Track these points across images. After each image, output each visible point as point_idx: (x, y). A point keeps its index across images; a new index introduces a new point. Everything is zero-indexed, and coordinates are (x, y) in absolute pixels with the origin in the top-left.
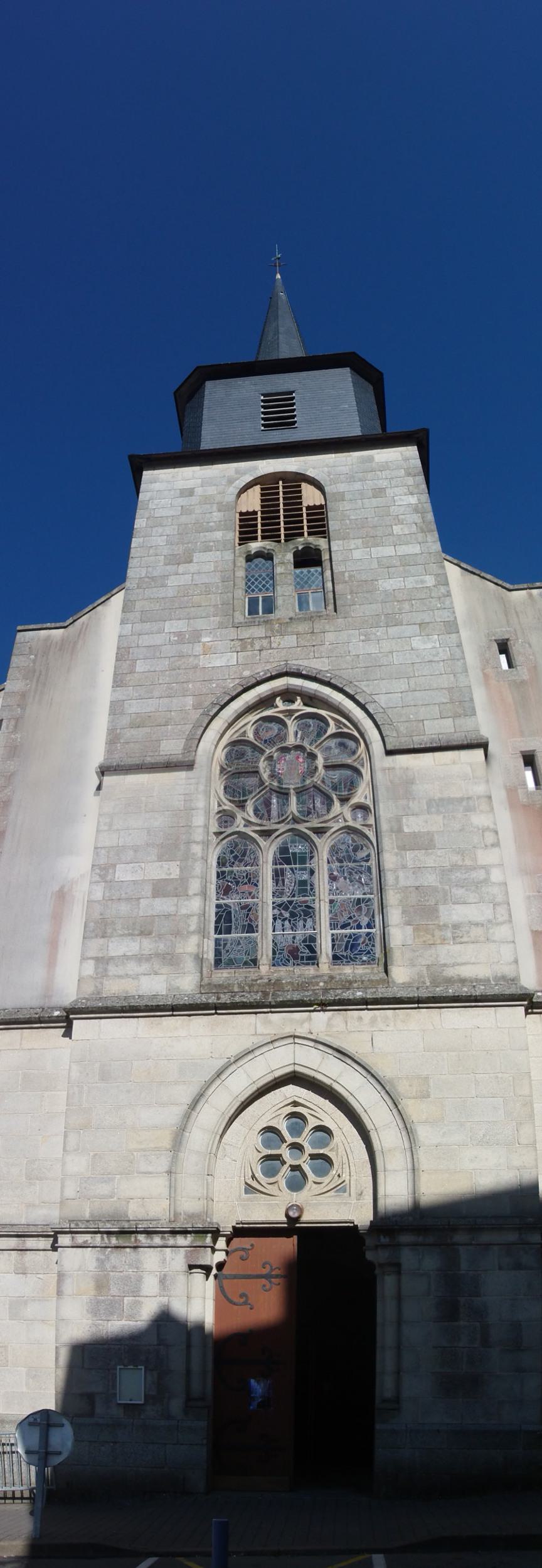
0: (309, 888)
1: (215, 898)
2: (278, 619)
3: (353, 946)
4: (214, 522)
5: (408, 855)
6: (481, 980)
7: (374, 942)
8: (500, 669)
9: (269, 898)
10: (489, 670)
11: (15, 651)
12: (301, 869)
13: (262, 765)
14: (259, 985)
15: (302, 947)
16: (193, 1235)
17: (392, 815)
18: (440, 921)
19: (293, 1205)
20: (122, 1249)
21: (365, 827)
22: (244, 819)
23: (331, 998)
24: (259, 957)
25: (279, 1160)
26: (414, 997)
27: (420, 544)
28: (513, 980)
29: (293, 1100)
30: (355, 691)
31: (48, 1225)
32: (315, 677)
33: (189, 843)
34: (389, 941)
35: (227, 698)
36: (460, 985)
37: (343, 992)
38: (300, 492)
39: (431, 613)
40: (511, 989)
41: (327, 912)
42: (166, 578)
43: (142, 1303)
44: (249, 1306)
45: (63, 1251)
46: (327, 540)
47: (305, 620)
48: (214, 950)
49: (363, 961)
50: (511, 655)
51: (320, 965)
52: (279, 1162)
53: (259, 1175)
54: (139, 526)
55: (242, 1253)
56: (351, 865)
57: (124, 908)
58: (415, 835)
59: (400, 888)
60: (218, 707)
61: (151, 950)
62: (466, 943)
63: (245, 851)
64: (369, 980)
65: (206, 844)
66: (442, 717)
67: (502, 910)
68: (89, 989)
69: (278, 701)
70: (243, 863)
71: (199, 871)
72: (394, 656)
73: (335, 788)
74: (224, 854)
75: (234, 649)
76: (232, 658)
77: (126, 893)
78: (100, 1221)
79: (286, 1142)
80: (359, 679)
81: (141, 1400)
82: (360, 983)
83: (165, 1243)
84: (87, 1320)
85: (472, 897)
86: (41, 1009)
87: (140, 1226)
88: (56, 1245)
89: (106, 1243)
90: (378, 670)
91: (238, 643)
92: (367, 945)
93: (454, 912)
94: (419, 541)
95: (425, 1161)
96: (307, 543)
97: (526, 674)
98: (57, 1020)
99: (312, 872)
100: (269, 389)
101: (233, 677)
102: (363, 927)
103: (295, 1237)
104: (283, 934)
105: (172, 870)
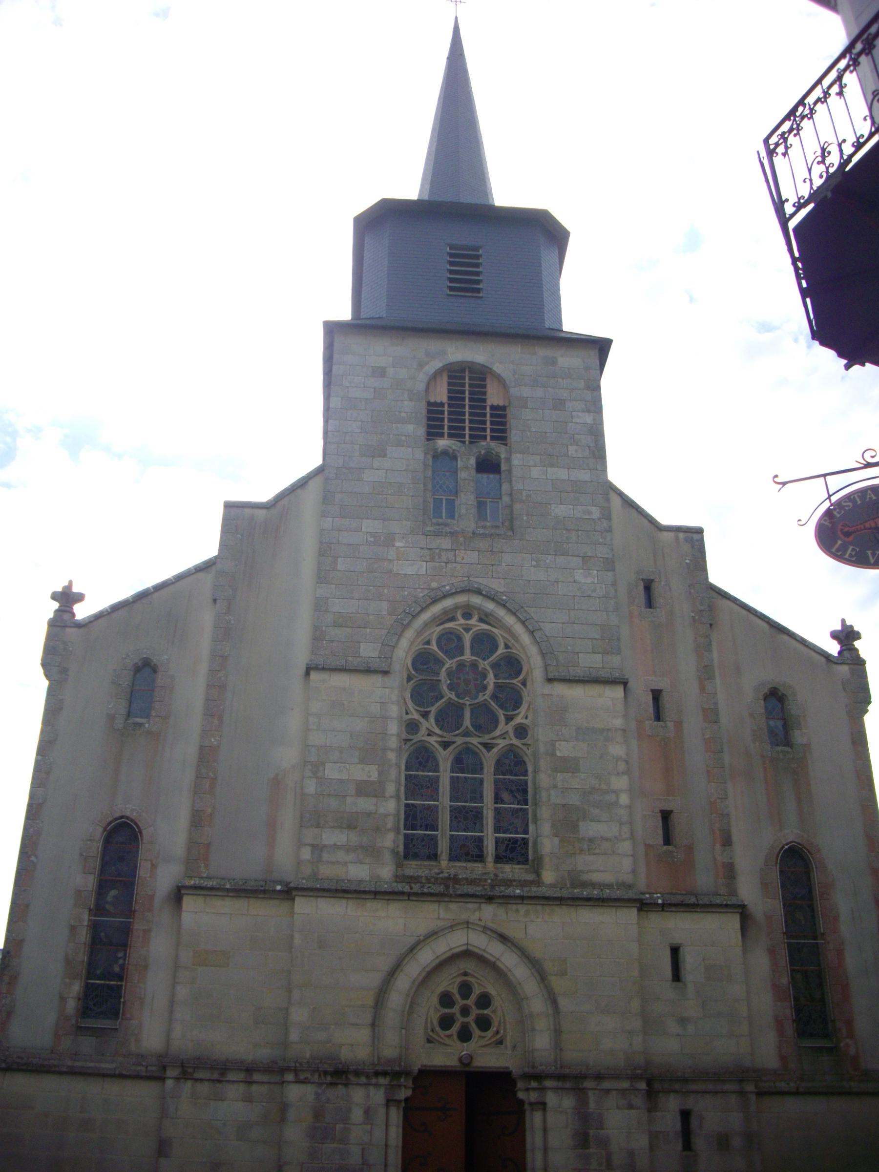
4: (405, 412)
14: (442, 879)
18: (579, 835)
24: (439, 853)
27: (590, 470)
33: (385, 749)
58: (564, 759)
66: (594, 652)
72: (560, 586)
76: (422, 568)
77: (335, 790)
97: (664, 617)
101: (422, 587)
105: (371, 773)
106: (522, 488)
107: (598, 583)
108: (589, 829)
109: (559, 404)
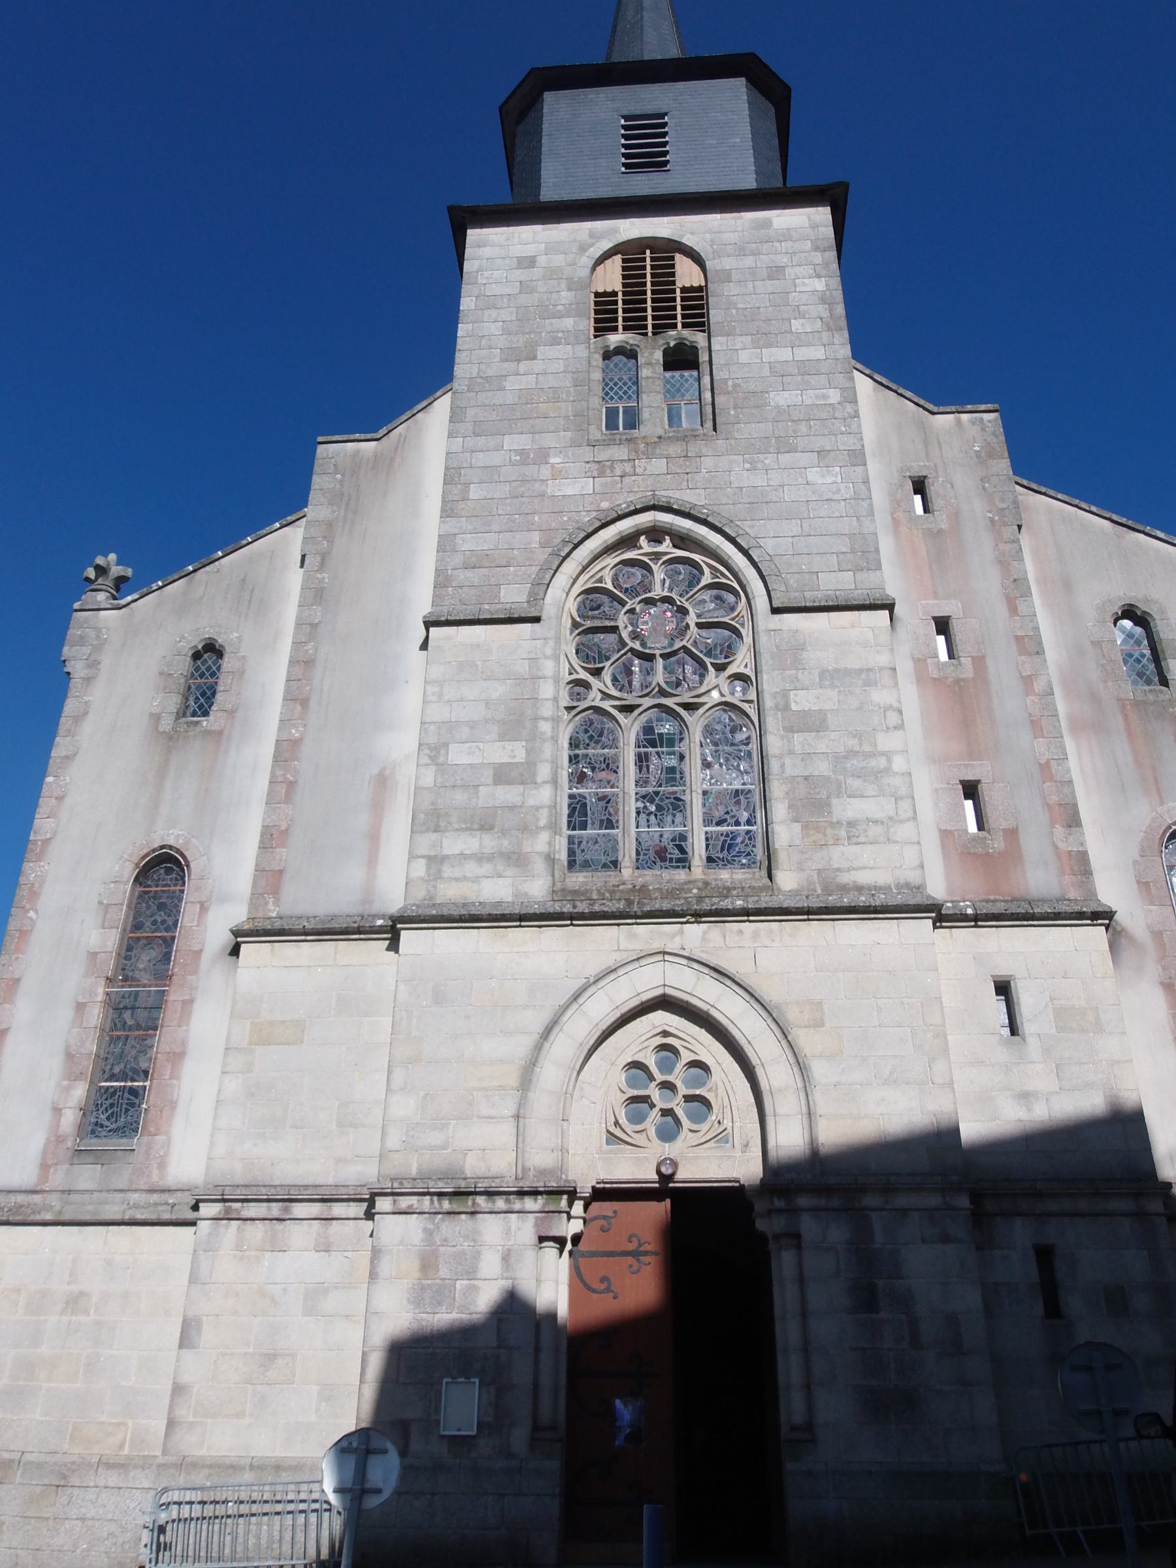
0: (678, 776)
1: (567, 787)
2: (644, 437)
3: (730, 847)
5: (795, 738)
6: (881, 888)
7: (755, 841)
8: (913, 514)
9: (631, 788)
10: (900, 515)
11: (316, 469)
12: (670, 754)
13: (622, 620)
14: (622, 891)
15: (670, 847)
16: (545, 1196)
17: (778, 690)
18: (832, 817)
19: (666, 1159)
20: (456, 1216)
21: (745, 704)
22: (600, 690)
23: (706, 908)
24: (620, 859)
25: (648, 1102)
26: (803, 907)
28: (918, 888)
29: (662, 1030)
30: (737, 532)
31: (364, 1186)
32: (689, 513)
33: (536, 719)
34: (773, 841)
35: (582, 535)
36: (856, 893)
37: (720, 901)
38: (673, 266)
39: (833, 438)
40: (916, 899)
41: (700, 806)
42: (503, 378)
43: (479, 1288)
44: (612, 1294)
45: (381, 1218)
46: (706, 334)
47: (677, 441)
48: (567, 850)
49: (742, 864)
50: (929, 497)
51: (692, 869)
52: (646, 1105)
53: (623, 1120)
54: (466, 308)
55: (603, 1222)
56: (728, 749)
57: (460, 797)
58: (804, 714)
59: (787, 779)
60: (571, 546)
61: (493, 847)
62: (863, 843)
63: (602, 729)
64: (750, 887)
65: (555, 720)
66: (841, 569)
67: (905, 805)
68: (419, 893)
69: (643, 540)
70: (600, 744)
71: (549, 755)
73: (709, 654)
74: (577, 733)
75: (589, 474)
76: (588, 486)
77: (462, 779)
78: (430, 1179)
79: (655, 1080)
80: (742, 518)
81: (472, 1431)
82: (740, 890)
83: (510, 1208)
84: (408, 1312)
85: (871, 789)
86: (360, 918)
87: (480, 1185)
88: (373, 1211)
89: (435, 1208)
90: (765, 507)
91: (595, 466)
92: (747, 845)
93: (848, 807)
94: (825, 342)
95: (822, 1104)
96: (680, 338)
98: (380, 930)
99: (682, 758)
100: (632, 108)
102: (742, 824)
103: (668, 1201)
104: (648, 831)
105: (517, 752)
106: (727, 377)
107: (842, 482)
108: (847, 809)
109: (776, 272)
